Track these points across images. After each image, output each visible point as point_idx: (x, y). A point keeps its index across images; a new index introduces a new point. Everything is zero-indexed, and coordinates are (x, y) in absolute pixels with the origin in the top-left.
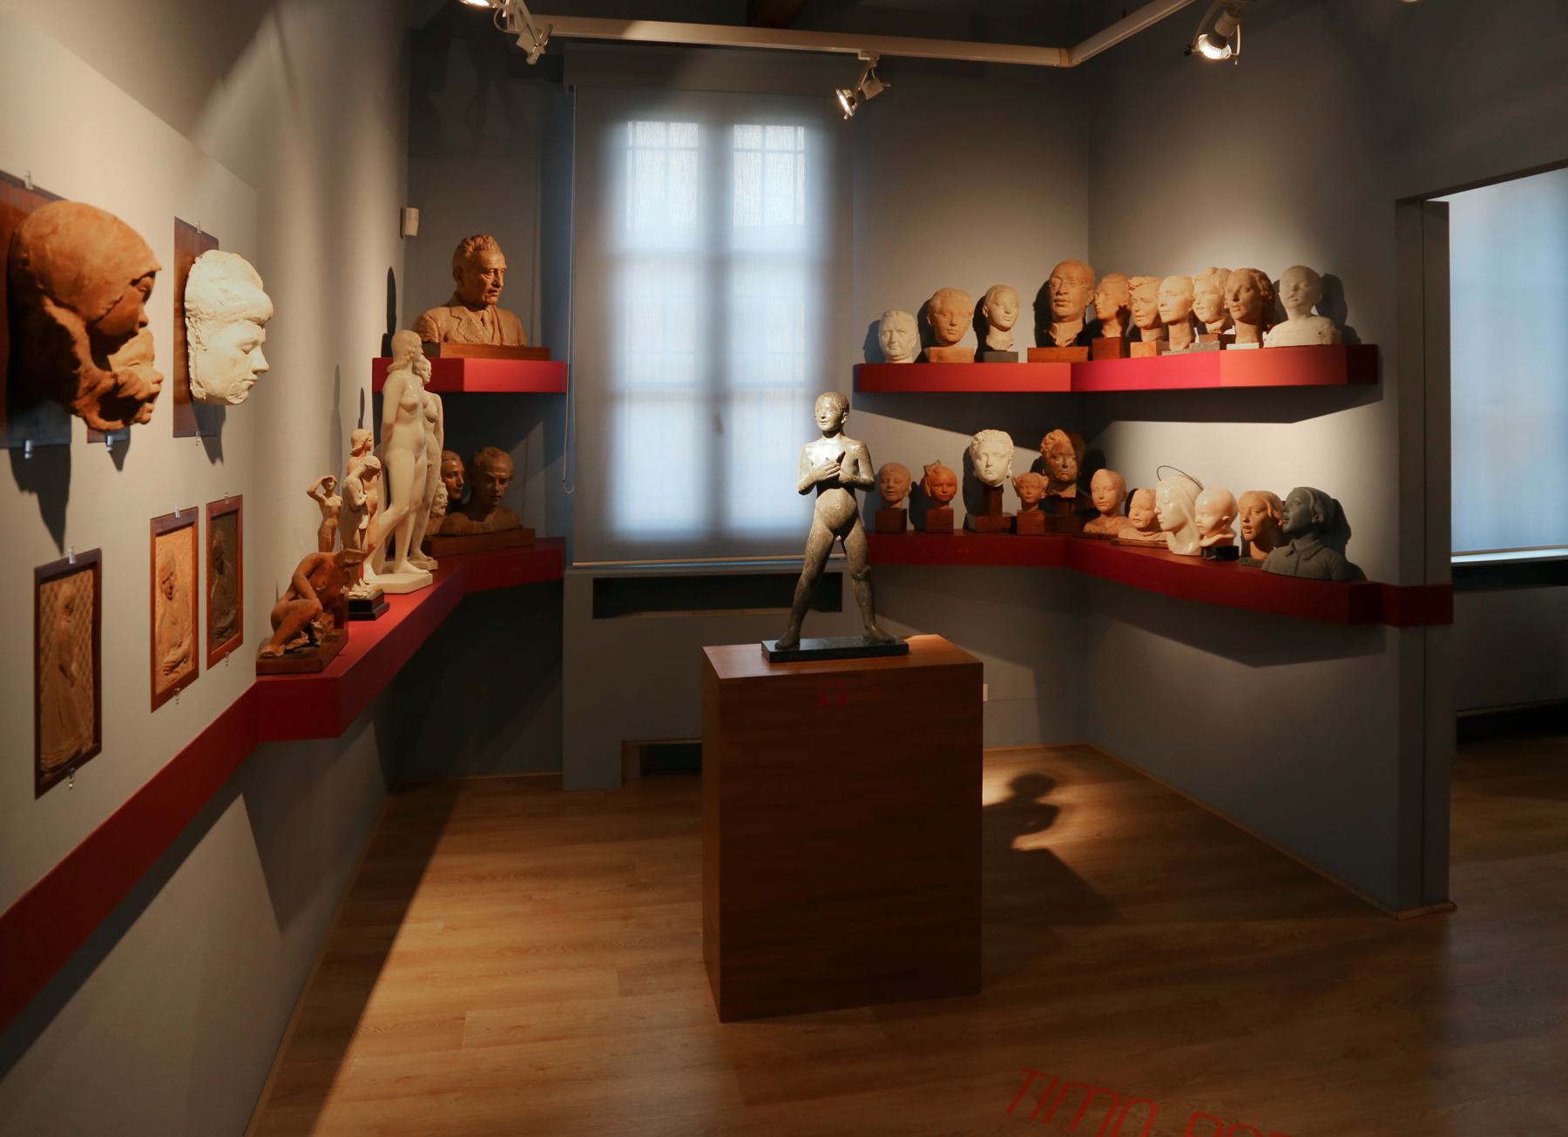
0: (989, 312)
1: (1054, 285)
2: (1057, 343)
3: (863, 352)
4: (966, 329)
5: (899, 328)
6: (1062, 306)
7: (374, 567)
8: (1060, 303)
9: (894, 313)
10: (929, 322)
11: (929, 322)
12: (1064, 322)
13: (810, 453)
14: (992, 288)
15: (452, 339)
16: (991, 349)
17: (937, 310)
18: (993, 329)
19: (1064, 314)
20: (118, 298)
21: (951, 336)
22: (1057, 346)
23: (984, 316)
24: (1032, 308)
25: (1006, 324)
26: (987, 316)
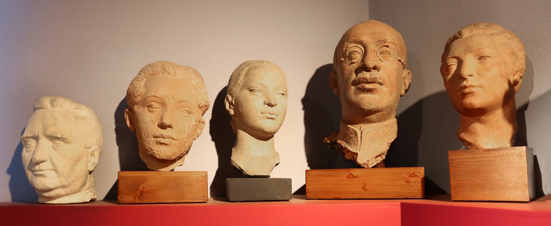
0: (237, 106)
1: (350, 58)
2: (360, 161)
3: (8, 177)
4: (194, 135)
5: (50, 132)
6: (370, 91)
7: (356, 80)
8: (368, 86)
9: (47, 102)
10: (128, 123)
11: (128, 123)
12: (369, 122)
13: (348, 73)
14: (245, 63)
15: (397, 92)
16: (239, 173)
17: (139, 99)
18: (244, 136)
19: (373, 107)
20: (149, 96)
21: (162, 147)
22: (359, 166)
23: (228, 112)
24: (301, 106)
25: (267, 125)
26: (232, 112)
